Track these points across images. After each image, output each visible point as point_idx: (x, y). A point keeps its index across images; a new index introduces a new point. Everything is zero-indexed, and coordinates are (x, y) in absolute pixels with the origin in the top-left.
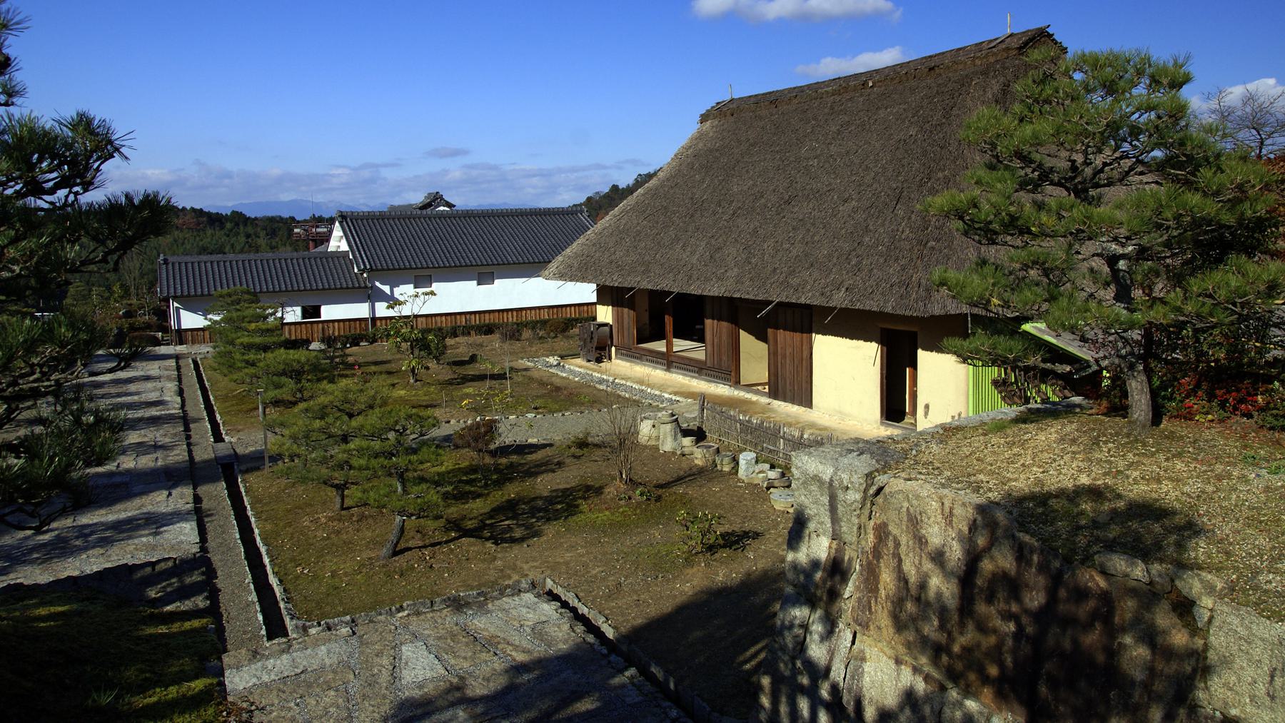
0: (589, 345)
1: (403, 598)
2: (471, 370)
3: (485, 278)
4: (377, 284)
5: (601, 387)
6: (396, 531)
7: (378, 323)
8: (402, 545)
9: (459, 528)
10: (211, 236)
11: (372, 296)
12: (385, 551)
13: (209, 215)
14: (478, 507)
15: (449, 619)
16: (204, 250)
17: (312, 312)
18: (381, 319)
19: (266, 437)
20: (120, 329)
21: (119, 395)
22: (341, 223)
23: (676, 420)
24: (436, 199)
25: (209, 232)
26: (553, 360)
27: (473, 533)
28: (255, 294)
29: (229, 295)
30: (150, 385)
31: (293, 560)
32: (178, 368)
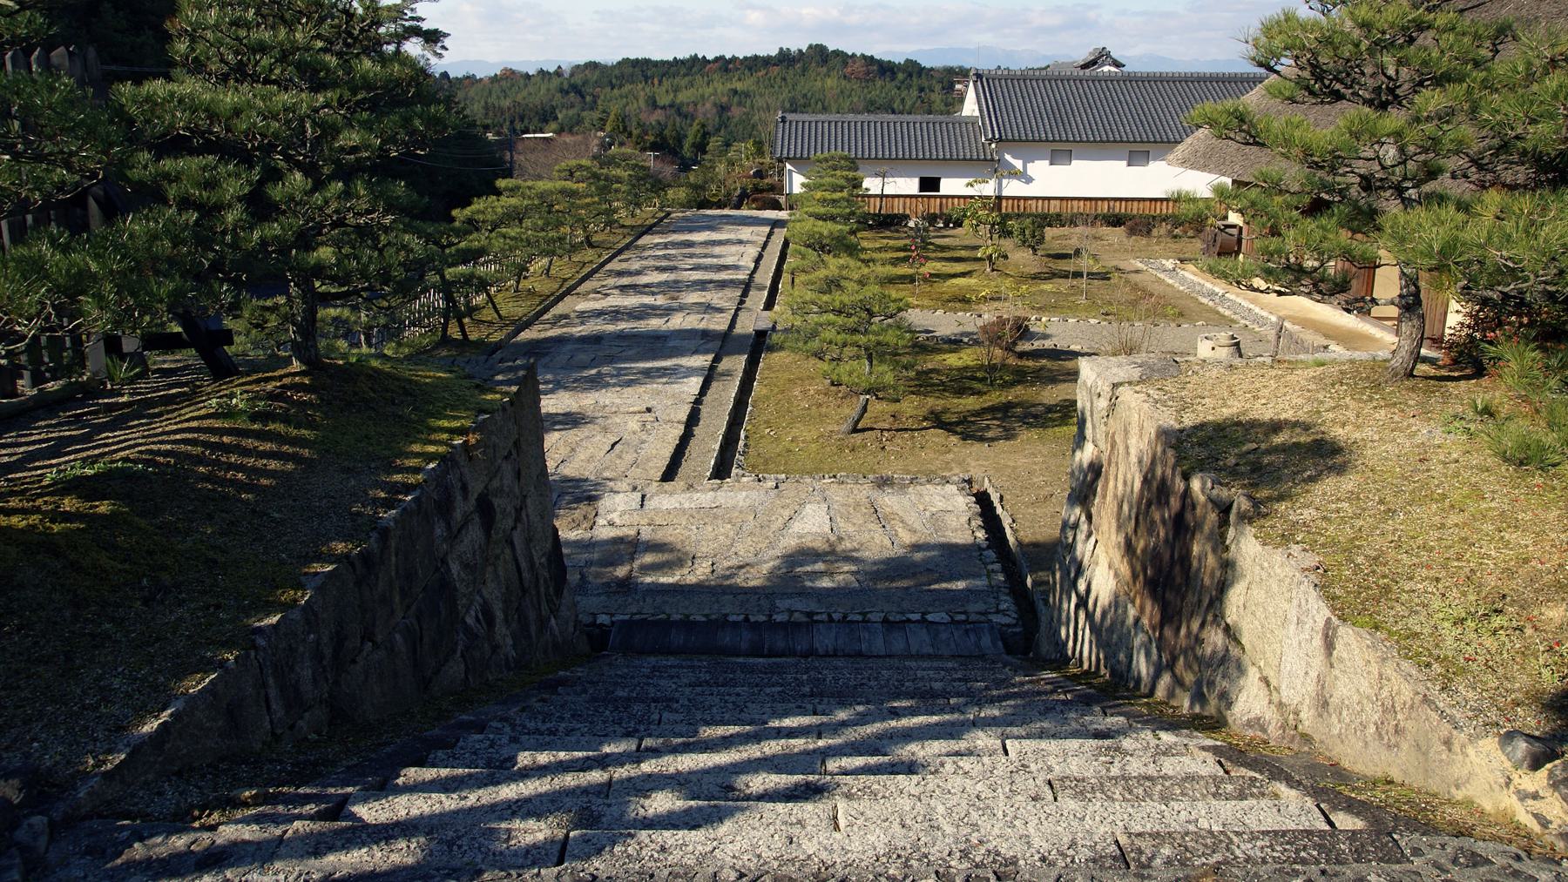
0: (1212, 249)
1: (840, 470)
2: (1063, 265)
3: (1138, 156)
4: (1008, 157)
5: (1205, 301)
6: (858, 409)
7: (1004, 203)
8: (860, 426)
9: (938, 421)
10: (881, 89)
11: (995, 167)
12: (846, 427)
13: (880, 63)
14: (970, 403)
15: (864, 491)
16: (872, 107)
17: (930, 184)
18: (1008, 198)
19: (497, 311)
20: (744, 189)
21: (706, 256)
22: (975, 82)
23: (1237, 344)
24: (1101, 57)
25: (879, 83)
26: (1169, 264)
27: (948, 427)
28: (853, 161)
29: (826, 160)
30: (734, 249)
31: (767, 422)
32: (769, 236)
